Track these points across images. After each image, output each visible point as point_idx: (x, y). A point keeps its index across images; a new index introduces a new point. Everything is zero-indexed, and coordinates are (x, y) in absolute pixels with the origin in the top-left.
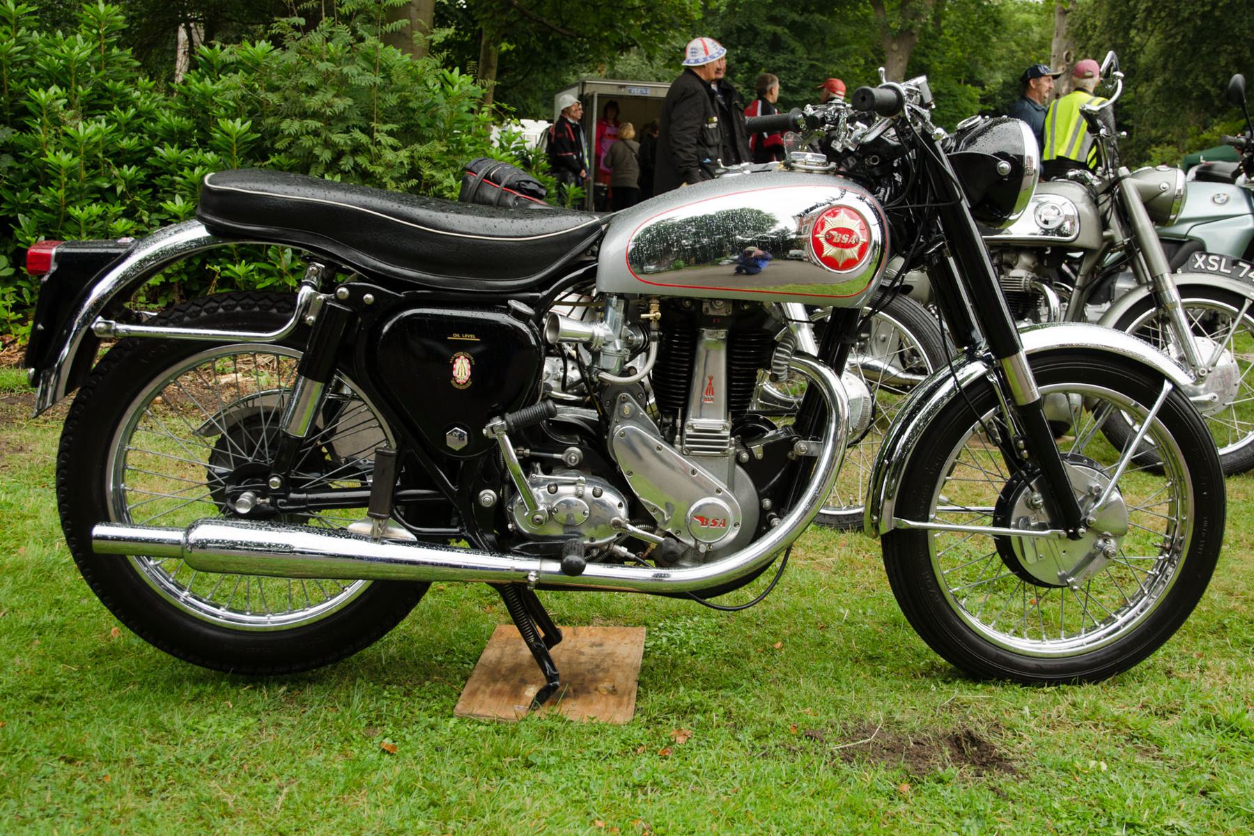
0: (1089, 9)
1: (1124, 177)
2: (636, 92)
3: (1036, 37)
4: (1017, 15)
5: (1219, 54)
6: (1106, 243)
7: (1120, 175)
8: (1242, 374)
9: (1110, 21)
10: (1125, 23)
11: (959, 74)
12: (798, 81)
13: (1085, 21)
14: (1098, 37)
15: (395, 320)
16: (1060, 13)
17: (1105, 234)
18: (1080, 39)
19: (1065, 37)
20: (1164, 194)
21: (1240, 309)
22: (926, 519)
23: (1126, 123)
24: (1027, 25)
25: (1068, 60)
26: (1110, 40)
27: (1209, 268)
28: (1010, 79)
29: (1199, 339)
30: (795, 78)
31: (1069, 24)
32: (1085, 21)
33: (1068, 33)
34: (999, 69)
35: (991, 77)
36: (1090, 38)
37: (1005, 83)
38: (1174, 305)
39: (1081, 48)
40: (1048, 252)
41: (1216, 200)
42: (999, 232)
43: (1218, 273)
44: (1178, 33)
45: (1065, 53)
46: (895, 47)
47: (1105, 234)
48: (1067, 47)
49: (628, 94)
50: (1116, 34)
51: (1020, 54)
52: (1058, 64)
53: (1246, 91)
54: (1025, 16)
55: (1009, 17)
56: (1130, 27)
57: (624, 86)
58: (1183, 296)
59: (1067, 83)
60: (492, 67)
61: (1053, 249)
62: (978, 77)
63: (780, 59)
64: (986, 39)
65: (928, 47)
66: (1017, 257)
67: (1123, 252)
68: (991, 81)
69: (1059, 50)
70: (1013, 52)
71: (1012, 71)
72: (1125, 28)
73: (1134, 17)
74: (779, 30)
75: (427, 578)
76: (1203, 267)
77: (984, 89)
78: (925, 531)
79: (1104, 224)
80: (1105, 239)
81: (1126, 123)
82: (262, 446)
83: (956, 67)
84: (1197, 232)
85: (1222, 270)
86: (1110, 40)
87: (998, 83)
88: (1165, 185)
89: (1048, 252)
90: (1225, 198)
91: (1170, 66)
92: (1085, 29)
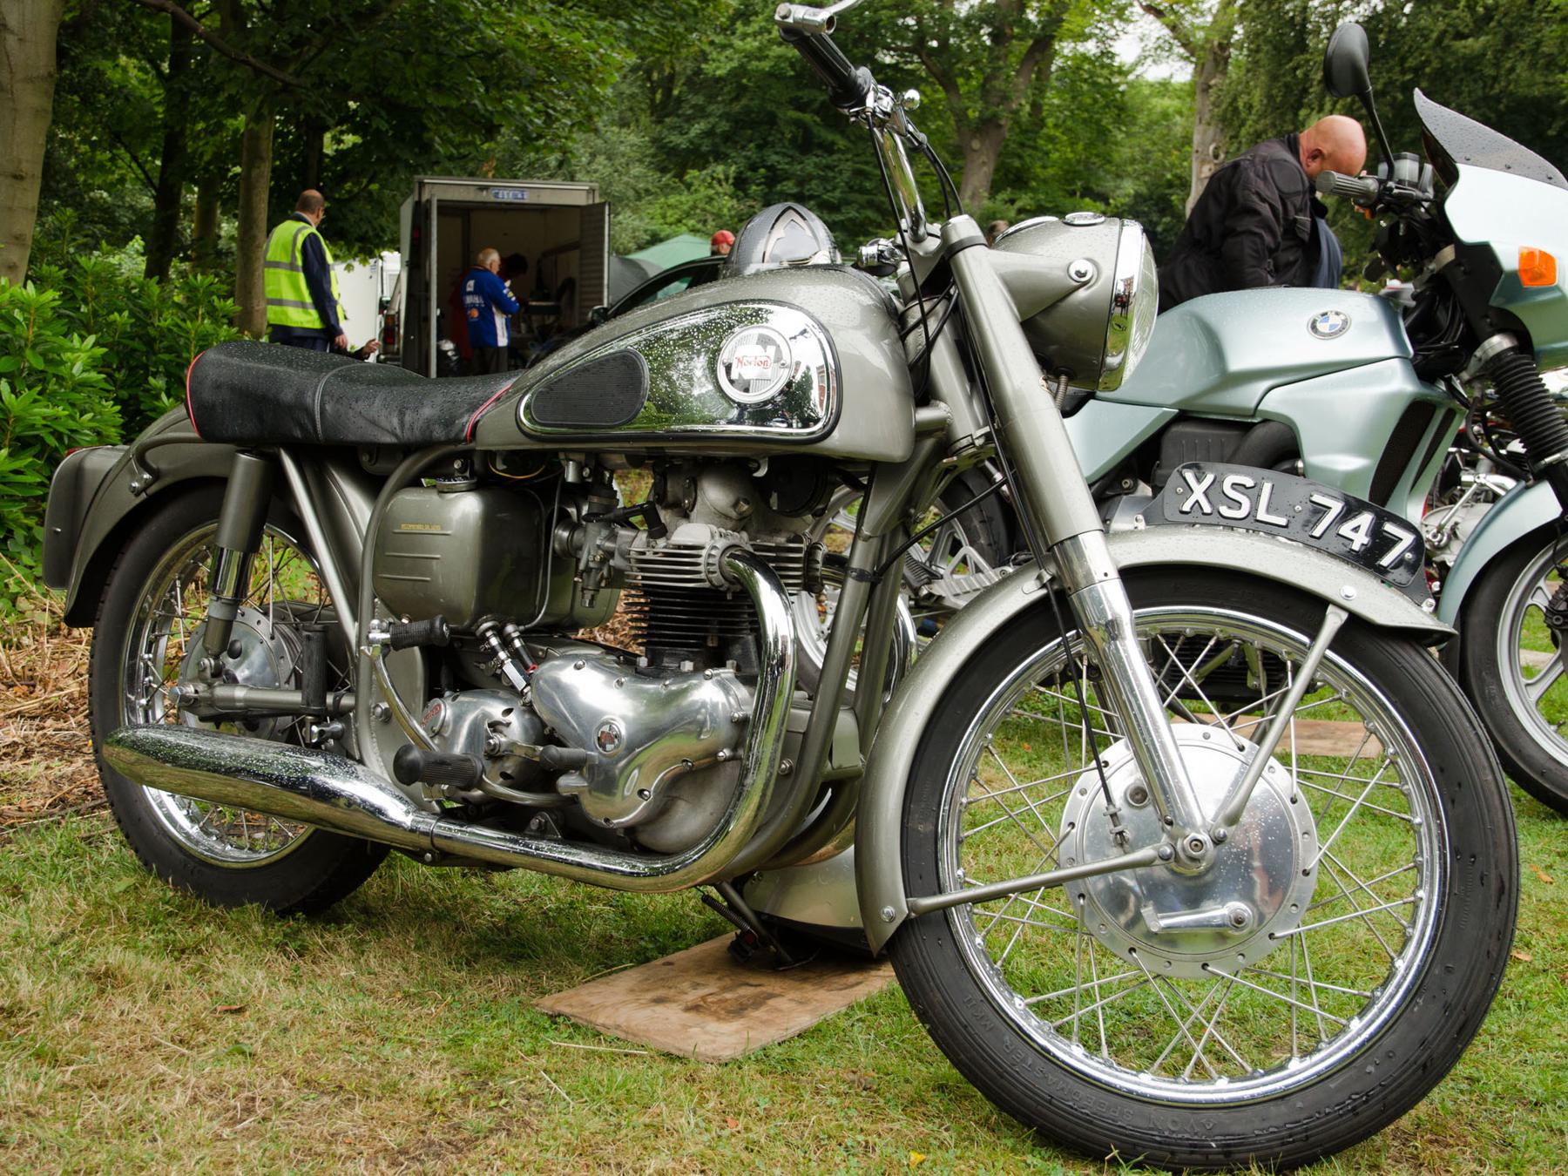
0: (1239, 83)
1: (963, 246)
2: (507, 196)
3: (1178, 131)
4: (1154, 101)
6: (929, 443)
7: (955, 239)
8: (1323, 838)
9: (1270, 97)
10: (1292, 100)
11: (1071, 182)
12: (837, 194)
13: (1235, 99)
14: (1256, 122)
17: (925, 414)
18: (1231, 125)
19: (1209, 124)
20: (1082, 294)
21: (1313, 636)
22: (940, 890)
24: (1165, 115)
25: (1216, 156)
26: (1274, 125)
27: (1224, 511)
28: (1144, 190)
29: (1182, 728)
30: (834, 189)
31: (1213, 104)
32: (1235, 99)
33: (1212, 117)
34: (1129, 175)
35: (1118, 187)
36: (1243, 124)
37: (1137, 195)
38: (1112, 629)
39: (1231, 138)
40: (762, 473)
41: (1321, 327)
43: (1252, 525)
45: (1212, 148)
46: (976, 144)
47: (925, 414)
49: (492, 199)
50: (1283, 115)
53: (1372, 61)
54: (1166, 102)
55: (1142, 103)
56: (1301, 106)
57: (486, 188)
58: (1136, 601)
60: (262, 159)
61: (774, 461)
62: (1097, 189)
63: (810, 164)
64: (1103, 133)
65: (1022, 145)
66: (694, 485)
68: (1118, 192)
69: (1205, 144)
70: (1148, 152)
71: (1147, 178)
72: (1292, 107)
73: (1305, 91)
74: (807, 117)
76: (1207, 508)
77: (1108, 204)
79: (922, 389)
80: (921, 432)
83: (1068, 172)
84: (1279, 401)
85: (1262, 515)
86: (1274, 125)
87: (1128, 195)
88: (1083, 266)
89: (762, 473)
90: (1337, 321)
92: (1236, 111)
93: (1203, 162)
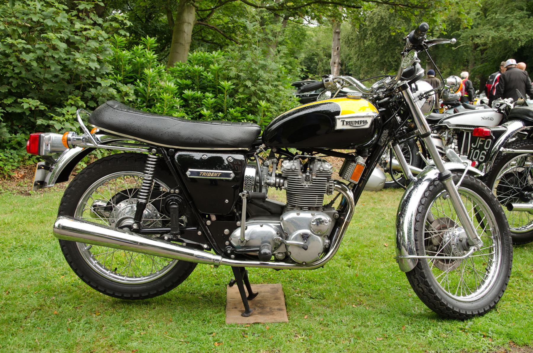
5: (395, 49)
15: (244, 149)
16: (335, 33)
23: (350, 73)
37: (305, 57)
42: (531, 128)
44: (382, 42)
45: (337, 48)
48: (337, 45)
51: (310, 47)
52: (335, 51)
59: (338, 58)
67: (517, 137)
71: (307, 53)
75: (196, 261)
78: (128, 189)
81: (350, 73)
82: (160, 197)
87: (303, 57)
91: (379, 54)
93: (335, 51)
